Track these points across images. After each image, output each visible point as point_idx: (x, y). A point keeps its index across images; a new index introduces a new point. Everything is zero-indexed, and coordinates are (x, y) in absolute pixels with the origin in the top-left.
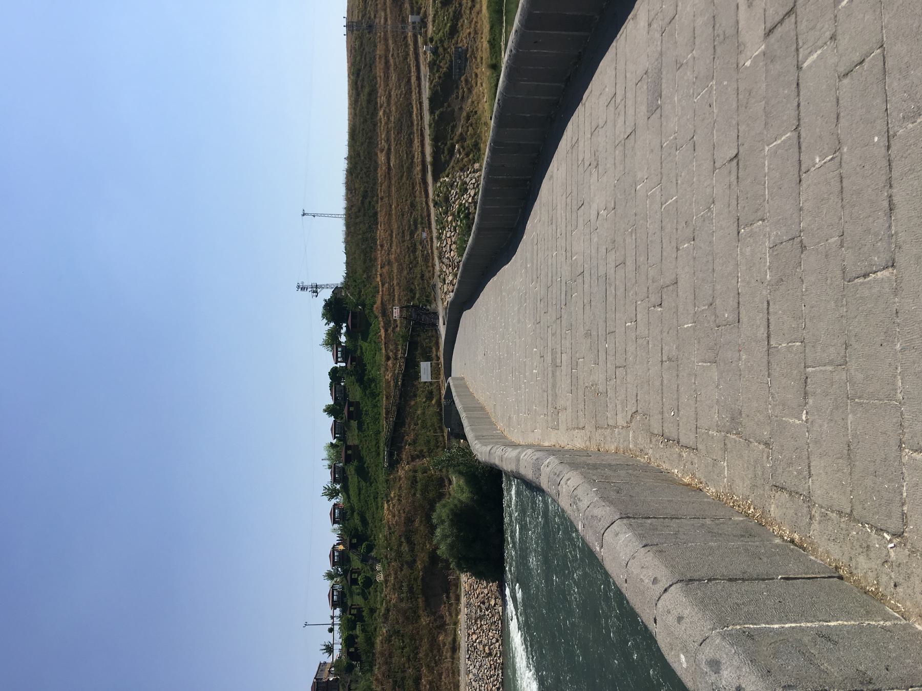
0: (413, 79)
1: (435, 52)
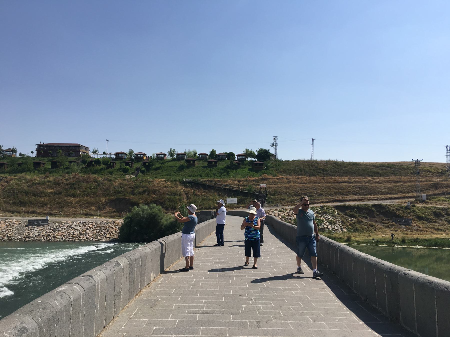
0: (390, 196)
1: (407, 208)
